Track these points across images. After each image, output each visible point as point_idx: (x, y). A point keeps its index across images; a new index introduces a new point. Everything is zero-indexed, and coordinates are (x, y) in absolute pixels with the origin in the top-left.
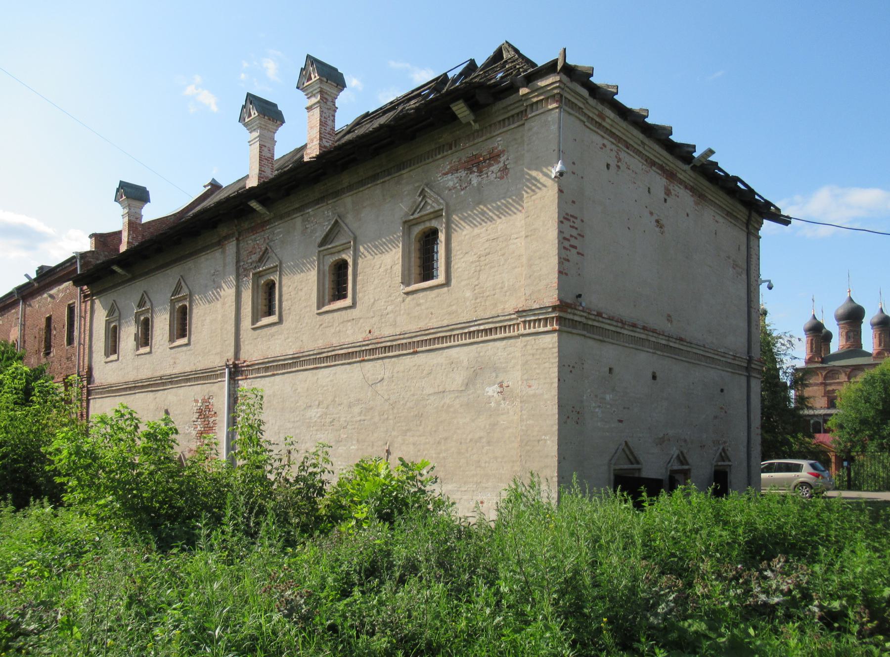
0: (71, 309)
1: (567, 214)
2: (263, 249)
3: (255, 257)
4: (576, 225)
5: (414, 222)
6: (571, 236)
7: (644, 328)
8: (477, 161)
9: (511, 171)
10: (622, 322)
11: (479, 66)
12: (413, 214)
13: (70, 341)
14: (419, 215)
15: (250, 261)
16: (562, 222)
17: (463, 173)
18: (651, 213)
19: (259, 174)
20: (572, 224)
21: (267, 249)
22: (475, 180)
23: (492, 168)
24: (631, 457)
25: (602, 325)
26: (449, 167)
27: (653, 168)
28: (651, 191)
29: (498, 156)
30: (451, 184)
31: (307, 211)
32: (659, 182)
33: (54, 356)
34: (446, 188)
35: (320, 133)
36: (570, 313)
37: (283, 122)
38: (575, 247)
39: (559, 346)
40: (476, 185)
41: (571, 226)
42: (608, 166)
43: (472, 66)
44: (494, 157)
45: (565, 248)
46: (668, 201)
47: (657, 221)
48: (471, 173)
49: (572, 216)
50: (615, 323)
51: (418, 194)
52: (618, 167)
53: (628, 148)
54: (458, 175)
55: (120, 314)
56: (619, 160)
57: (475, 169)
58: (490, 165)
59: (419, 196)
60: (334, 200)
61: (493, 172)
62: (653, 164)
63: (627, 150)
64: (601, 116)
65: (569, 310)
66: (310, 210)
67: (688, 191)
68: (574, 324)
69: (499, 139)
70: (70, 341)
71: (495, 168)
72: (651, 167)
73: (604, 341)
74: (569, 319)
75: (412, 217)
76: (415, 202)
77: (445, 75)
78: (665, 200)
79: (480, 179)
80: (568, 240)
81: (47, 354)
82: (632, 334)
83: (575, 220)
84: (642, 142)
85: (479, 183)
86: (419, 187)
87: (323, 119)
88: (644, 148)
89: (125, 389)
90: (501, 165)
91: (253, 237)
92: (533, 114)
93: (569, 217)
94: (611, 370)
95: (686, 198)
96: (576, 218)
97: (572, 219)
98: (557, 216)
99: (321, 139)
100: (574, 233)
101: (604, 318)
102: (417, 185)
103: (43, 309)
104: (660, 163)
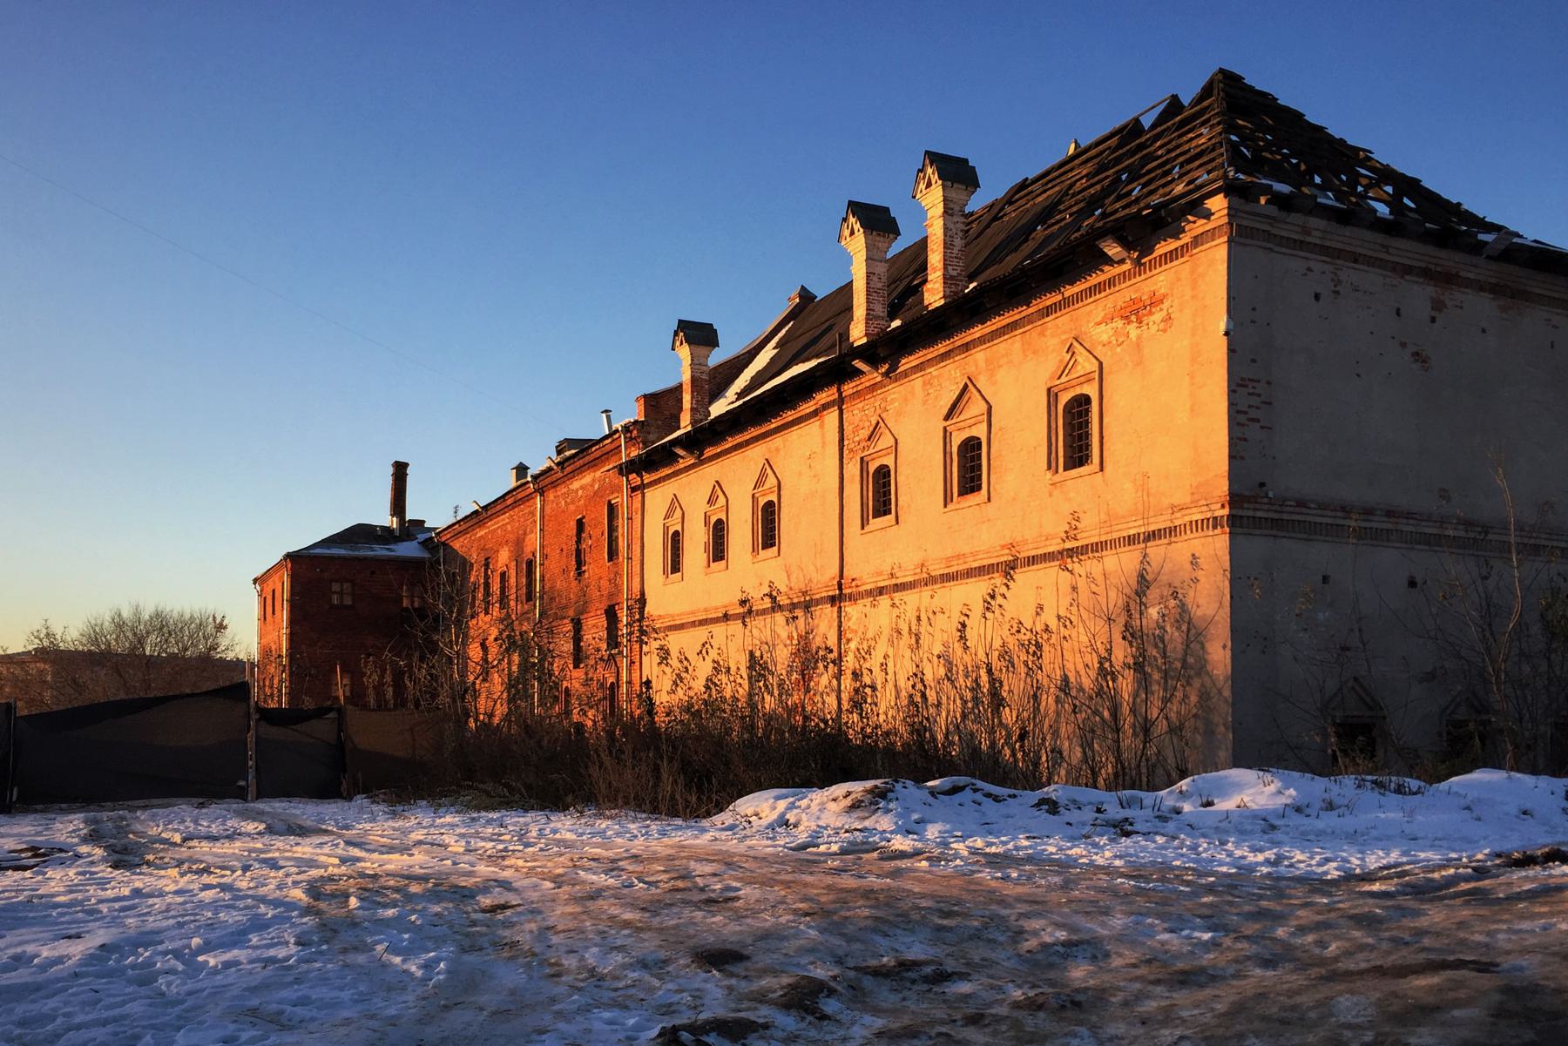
0: (612, 509)
1: (1243, 379)
2: (874, 423)
3: (865, 433)
4: (1256, 391)
5: (1062, 387)
6: (1250, 406)
7: (1389, 513)
8: (1136, 307)
9: (1175, 322)
10: (1343, 509)
11: (1186, 104)
12: (1059, 378)
13: (613, 553)
14: (1067, 379)
15: (857, 439)
16: (1234, 391)
17: (1119, 323)
18: (1403, 345)
19: (867, 314)
20: (1251, 391)
21: (878, 423)
22: (1133, 331)
23: (1152, 318)
24: (1368, 700)
25: (1309, 518)
26: (1102, 314)
27: (1407, 277)
28: (1403, 312)
29: (1161, 301)
30: (1105, 338)
31: (929, 370)
32: (1418, 295)
33: (589, 578)
34: (1099, 343)
35: (945, 260)
36: (1248, 509)
37: (898, 234)
38: (1258, 421)
39: (1230, 553)
40: (1134, 339)
41: (1249, 394)
42: (1317, 297)
43: (1174, 105)
44: (1155, 301)
45: (1239, 424)
46: (1437, 319)
47: (1416, 354)
48: (1128, 323)
49: (1252, 380)
50: (1329, 513)
51: (1066, 350)
52: (1337, 293)
53: (1356, 261)
54: (1114, 325)
55: (683, 514)
56: (1338, 283)
57: (1133, 318)
58: (1151, 313)
59: (1067, 352)
60: (963, 356)
61: (1154, 323)
62: (1407, 270)
63: (1356, 266)
64: (1307, 232)
65: (1246, 505)
66: (932, 369)
67: (1486, 294)
68: (1256, 522)
69: (1161, 278)
70: (613, 553)
71: (1158, 317)
72: (1402, 277)
73: (1310, 540)
74: (1248, 517)
75: (1058, 382)
76: (1061, 361)
77: (1137, 121)
78: (1433, 320)
79: (1139, 331)
80: (1246, 413)
81: (580, 574)
82: (1368, 525)
83: (1255, 384)
84: (1383, 246)
85: (1139, 337)
86: (1067, 339)
87: (948, 238)
88: (1388, 252)
89: (693, 624)
90: (1164, 313)
91: (861, 405)
92: (1197, 250)
93: (1247, 382)
94: (1325, 579)
95: (1481, 306)
96: (1259, 381)
97: (1251, 384)
98: (1226, 384)
99: (945, 268)
100: (1255, 401)
101: (1310, 508)
102: (1064, 337)
103: (572, 507)
104: (1423, 265)
